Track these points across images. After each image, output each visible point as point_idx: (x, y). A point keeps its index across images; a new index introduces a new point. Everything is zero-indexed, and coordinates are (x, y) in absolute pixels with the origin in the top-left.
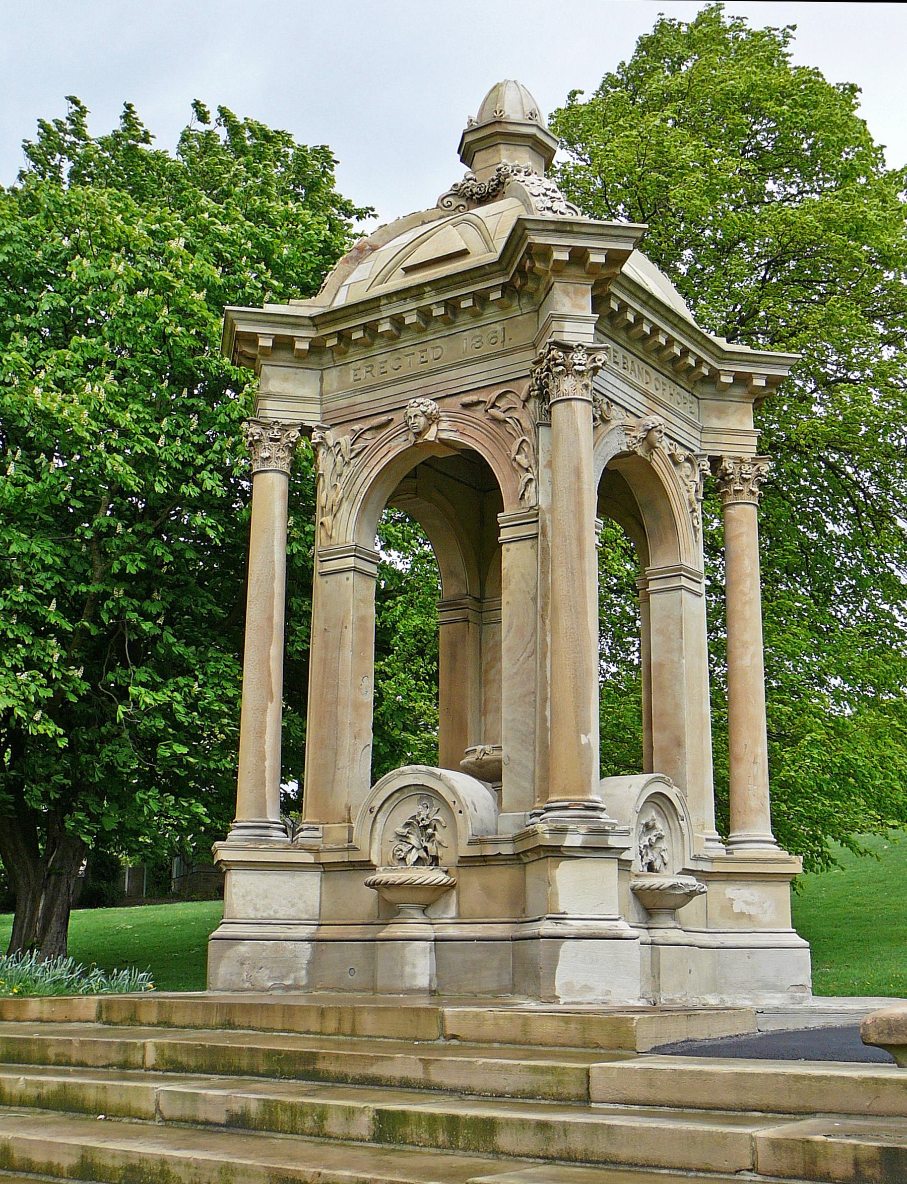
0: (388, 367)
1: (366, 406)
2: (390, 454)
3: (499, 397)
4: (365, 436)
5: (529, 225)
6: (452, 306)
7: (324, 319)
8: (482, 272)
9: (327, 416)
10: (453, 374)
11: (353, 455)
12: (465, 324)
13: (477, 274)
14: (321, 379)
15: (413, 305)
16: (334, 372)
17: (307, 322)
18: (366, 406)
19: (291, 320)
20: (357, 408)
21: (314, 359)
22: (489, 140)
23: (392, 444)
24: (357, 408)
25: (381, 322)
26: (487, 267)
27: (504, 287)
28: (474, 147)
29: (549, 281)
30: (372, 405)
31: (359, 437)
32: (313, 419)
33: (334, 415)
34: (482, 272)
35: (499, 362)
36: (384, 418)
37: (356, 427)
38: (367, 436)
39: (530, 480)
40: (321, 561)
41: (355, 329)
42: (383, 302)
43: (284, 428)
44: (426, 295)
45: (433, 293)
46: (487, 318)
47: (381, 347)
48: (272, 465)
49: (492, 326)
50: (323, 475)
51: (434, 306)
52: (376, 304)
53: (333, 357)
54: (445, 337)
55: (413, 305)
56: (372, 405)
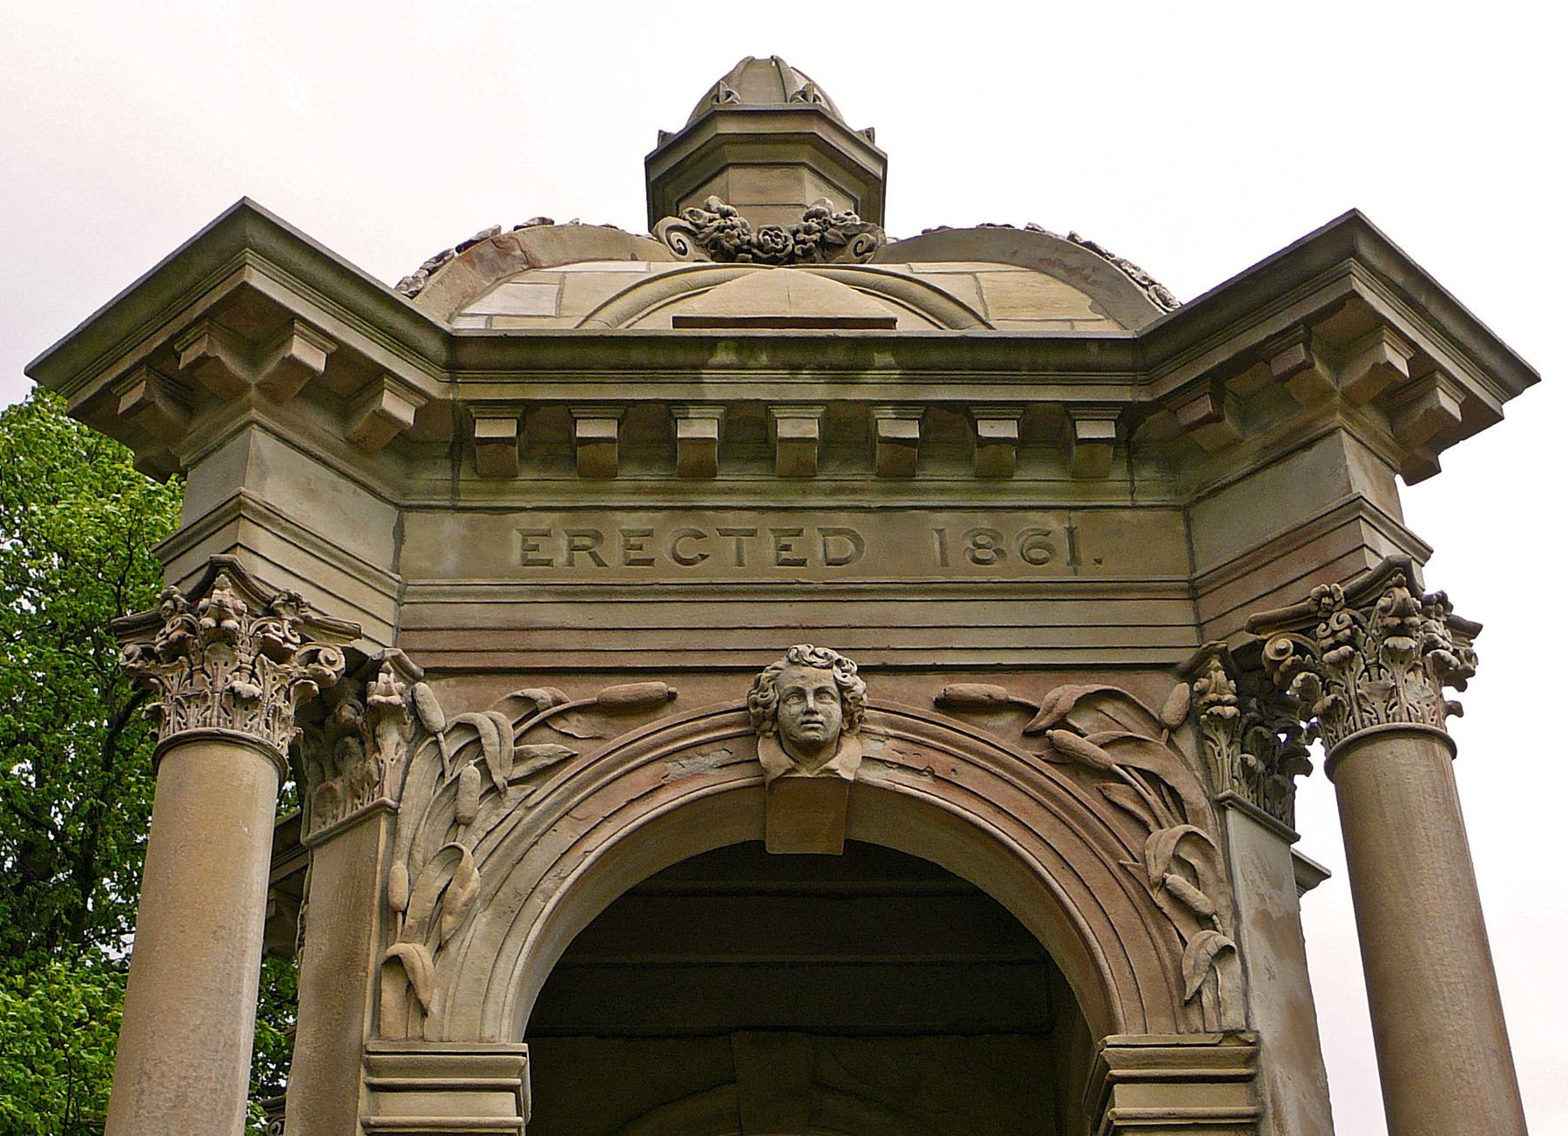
0: (660, 550)
1: (575, 640)
2: (663, 796)
3: (1087, 702)
4: (561, 725)
5: (1365, 249)
6: (948, 428)
7: (496, 356)
8: (1075, 357)
9: (419, 641)
10: (905, 612)
11: (521, 771)
12: (942, 491)
13: (1054, 357)
14: (399, 535)
15: (820, 392)
16: (450, 526)
17: (433, 346)
18: (575, 640)
19: (400, 323)
20: (539, 640)
21: (391, 466)
22: (782, 148)
23: (673, 768)
24: (539, 640)
25: (693, 412)
26: (1094, 349)
27: (1128, 417)
28: (732, 153)
29: (1309, 425)
30: (598, 641)
31: (543, 723)
32: (377, 641)
33: (443, 640)
34: (1075, 357)
35: (1066, 612)
36: (657, 686)
37: (541, 692)
38: (572, 726)
39: (1225, 952)
40: (373, 1088)
41: (589, 411)
42: (721, 357)
43: (311, 627)
44: (869, 376)
45: (896, 374)
46: (1020, 491)
47: (637, 491)
48: (254, 728)
49: (1031, 515)
50: (393, 813)
51: (889, 412)
52: (693, 357)
53: (455, 479)
54: (868, 510)
55: (820, 392)
56: (598, 641)
